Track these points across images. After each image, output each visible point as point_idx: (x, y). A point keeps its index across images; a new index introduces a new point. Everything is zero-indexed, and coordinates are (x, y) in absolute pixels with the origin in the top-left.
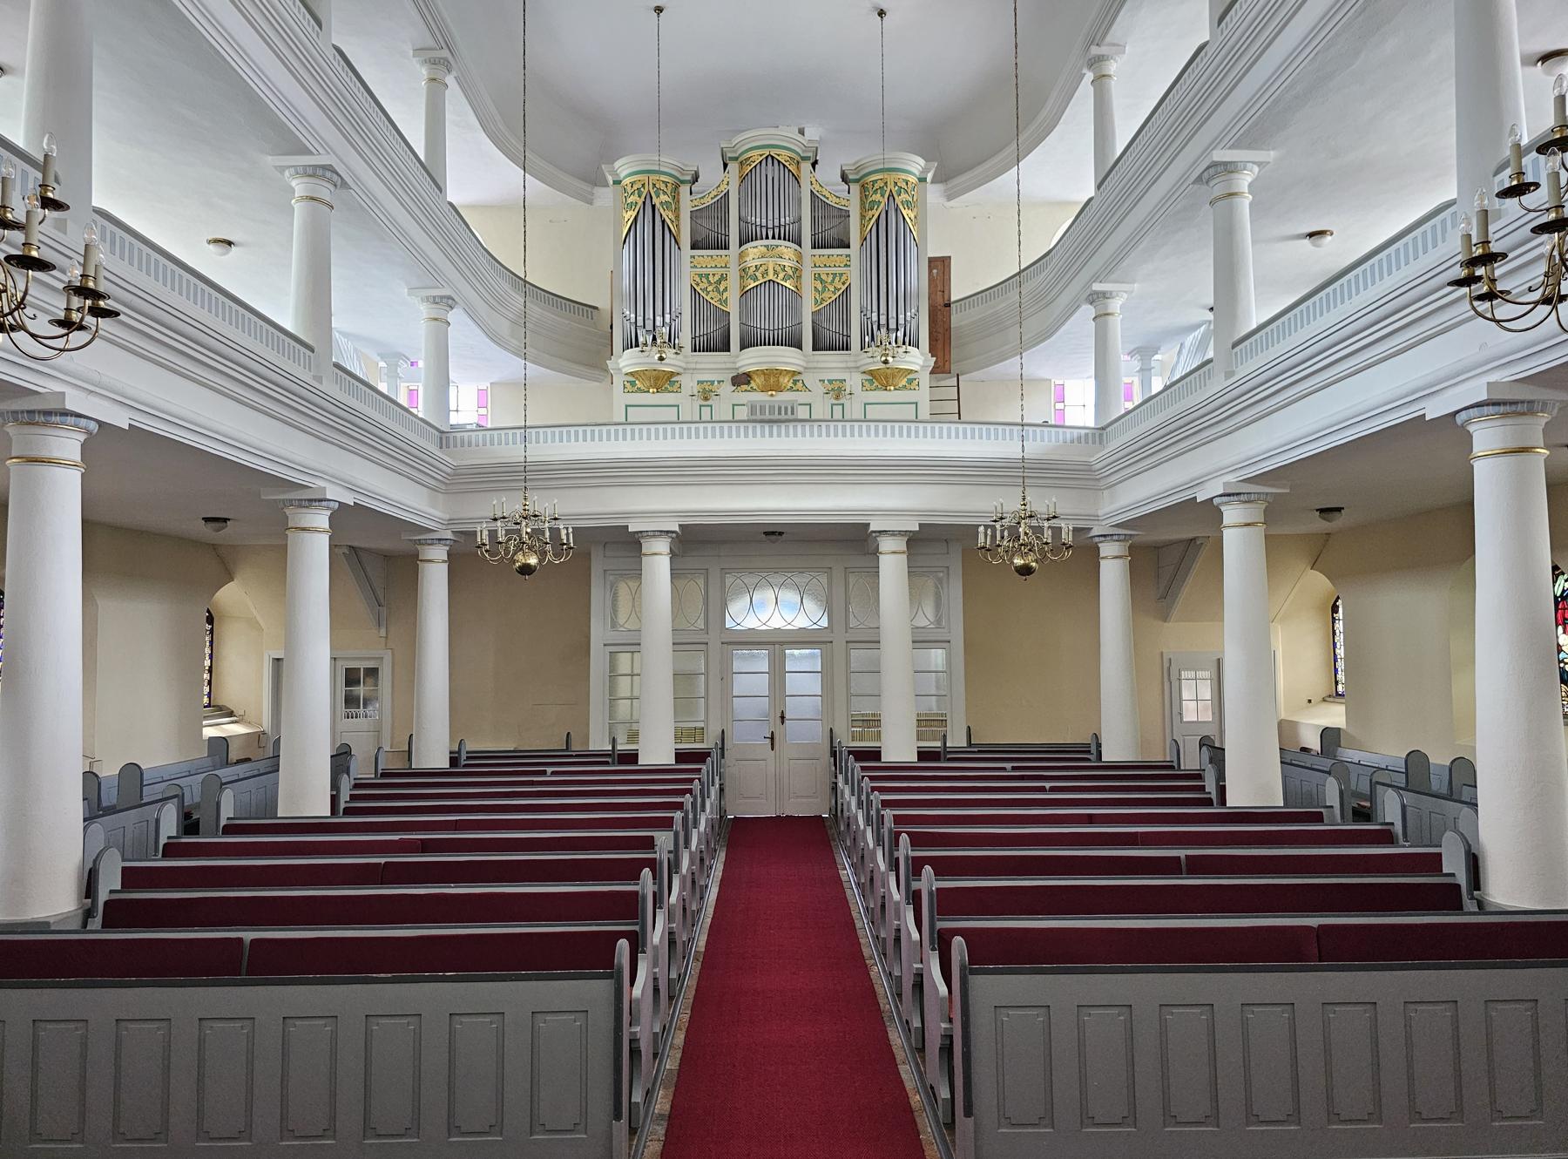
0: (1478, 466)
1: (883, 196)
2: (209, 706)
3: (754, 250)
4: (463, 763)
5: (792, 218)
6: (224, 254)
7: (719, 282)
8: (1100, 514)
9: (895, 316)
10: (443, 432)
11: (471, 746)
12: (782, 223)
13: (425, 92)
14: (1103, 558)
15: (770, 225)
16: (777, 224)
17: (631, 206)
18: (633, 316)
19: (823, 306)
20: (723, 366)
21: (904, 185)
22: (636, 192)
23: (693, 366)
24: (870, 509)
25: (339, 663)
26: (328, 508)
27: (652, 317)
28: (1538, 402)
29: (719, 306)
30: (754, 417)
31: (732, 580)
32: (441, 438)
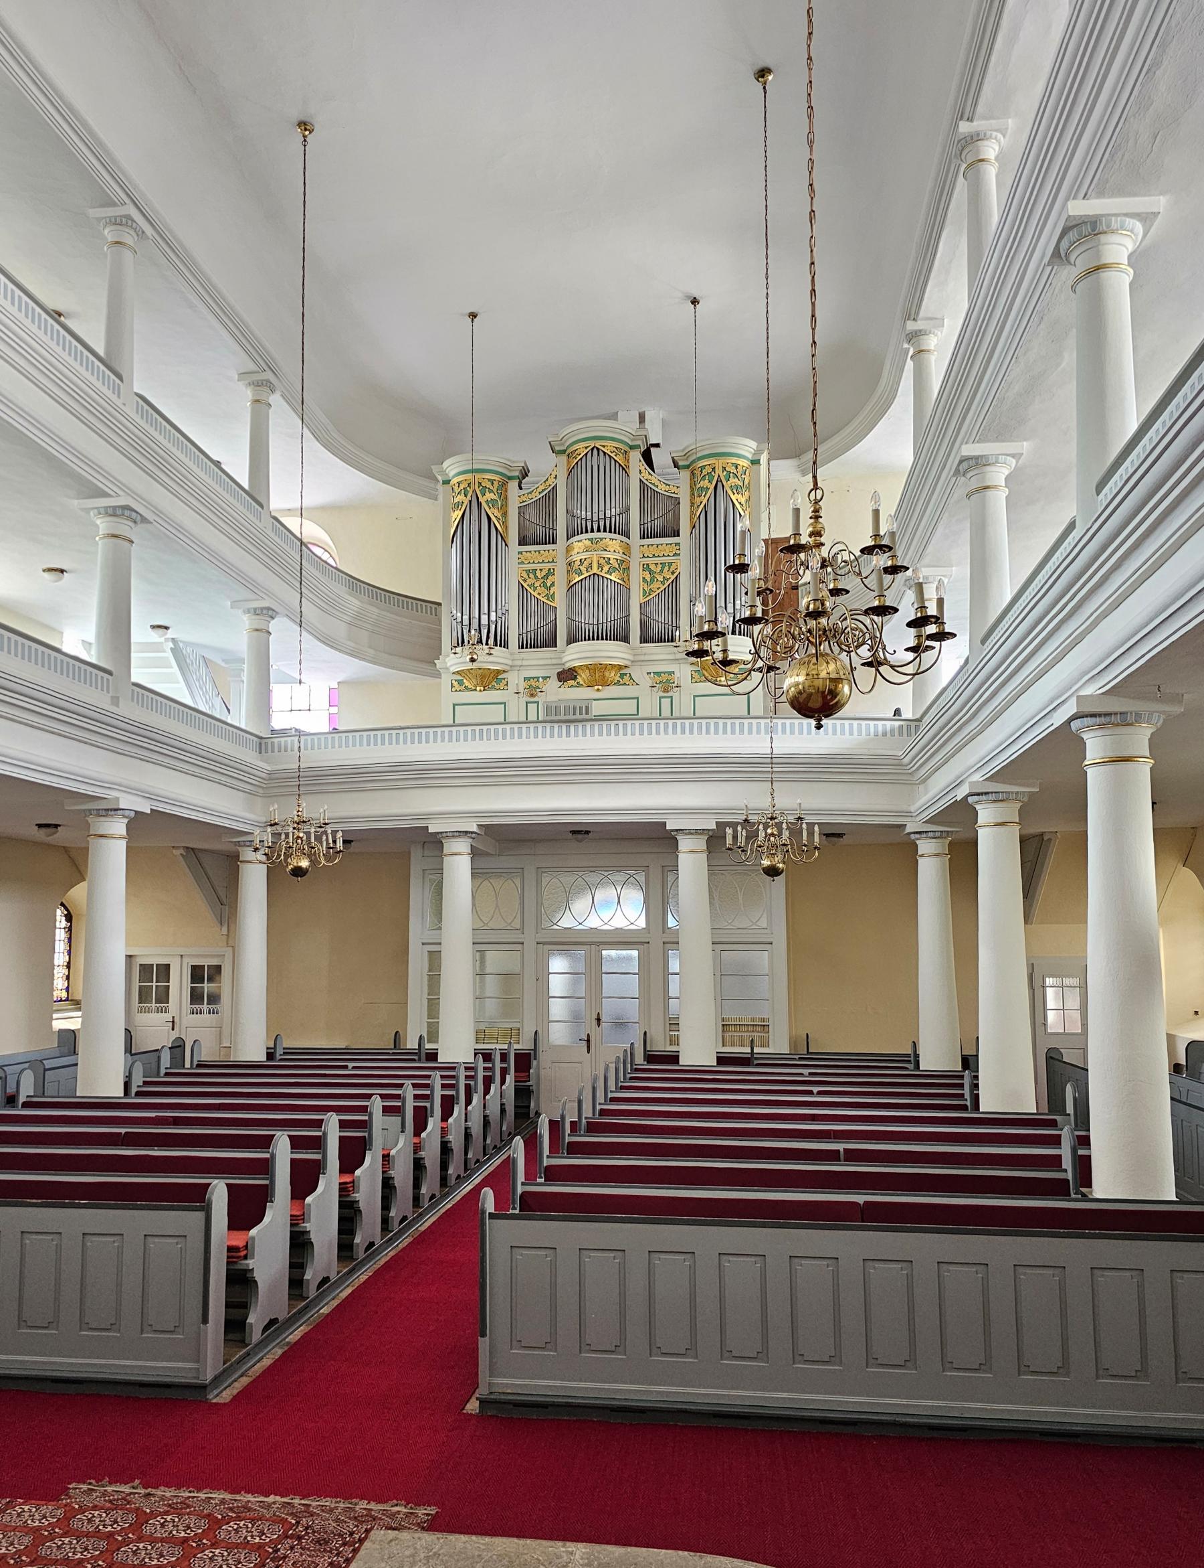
0: (1091, 772)
1: (710, 482)
2: (67, 999)
3: (580, 543)
4: (278, 1057)
5: (618, 510)
6: (56, 581)
7: (547, 576)
8: (912, 811)
9: (724, 606)
10: (261, 738)
11: (288, 1043)
12: (608, 515)
13: (249, 410)
14: (922, 856)
15: (595, 518)
16: (602, 516)
17: (458, 506)
18: (459, 615)
19: (651, 597)
20: (549, 662)
21: (733, 470)
22: (463, 491)
23: (519, 663)
24: (634, 808)
25: (185, 960)
26: (124, 816)
27: (477, 616)
28: (1131, 713)
29: (545, 601)
30: (549, 718)
31: (548, 879)
32: (260, 744)
